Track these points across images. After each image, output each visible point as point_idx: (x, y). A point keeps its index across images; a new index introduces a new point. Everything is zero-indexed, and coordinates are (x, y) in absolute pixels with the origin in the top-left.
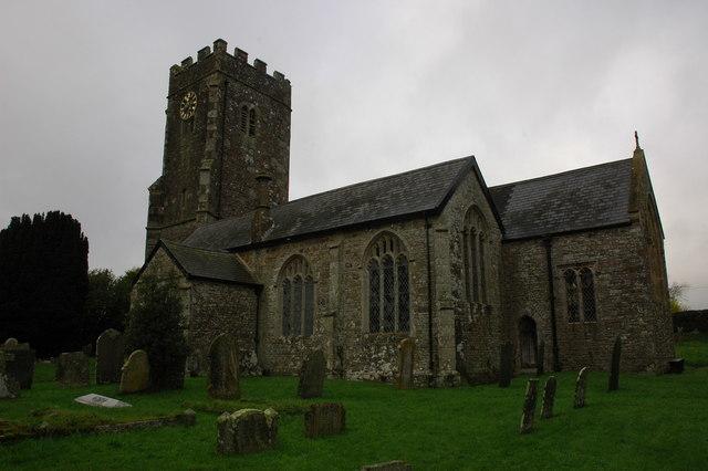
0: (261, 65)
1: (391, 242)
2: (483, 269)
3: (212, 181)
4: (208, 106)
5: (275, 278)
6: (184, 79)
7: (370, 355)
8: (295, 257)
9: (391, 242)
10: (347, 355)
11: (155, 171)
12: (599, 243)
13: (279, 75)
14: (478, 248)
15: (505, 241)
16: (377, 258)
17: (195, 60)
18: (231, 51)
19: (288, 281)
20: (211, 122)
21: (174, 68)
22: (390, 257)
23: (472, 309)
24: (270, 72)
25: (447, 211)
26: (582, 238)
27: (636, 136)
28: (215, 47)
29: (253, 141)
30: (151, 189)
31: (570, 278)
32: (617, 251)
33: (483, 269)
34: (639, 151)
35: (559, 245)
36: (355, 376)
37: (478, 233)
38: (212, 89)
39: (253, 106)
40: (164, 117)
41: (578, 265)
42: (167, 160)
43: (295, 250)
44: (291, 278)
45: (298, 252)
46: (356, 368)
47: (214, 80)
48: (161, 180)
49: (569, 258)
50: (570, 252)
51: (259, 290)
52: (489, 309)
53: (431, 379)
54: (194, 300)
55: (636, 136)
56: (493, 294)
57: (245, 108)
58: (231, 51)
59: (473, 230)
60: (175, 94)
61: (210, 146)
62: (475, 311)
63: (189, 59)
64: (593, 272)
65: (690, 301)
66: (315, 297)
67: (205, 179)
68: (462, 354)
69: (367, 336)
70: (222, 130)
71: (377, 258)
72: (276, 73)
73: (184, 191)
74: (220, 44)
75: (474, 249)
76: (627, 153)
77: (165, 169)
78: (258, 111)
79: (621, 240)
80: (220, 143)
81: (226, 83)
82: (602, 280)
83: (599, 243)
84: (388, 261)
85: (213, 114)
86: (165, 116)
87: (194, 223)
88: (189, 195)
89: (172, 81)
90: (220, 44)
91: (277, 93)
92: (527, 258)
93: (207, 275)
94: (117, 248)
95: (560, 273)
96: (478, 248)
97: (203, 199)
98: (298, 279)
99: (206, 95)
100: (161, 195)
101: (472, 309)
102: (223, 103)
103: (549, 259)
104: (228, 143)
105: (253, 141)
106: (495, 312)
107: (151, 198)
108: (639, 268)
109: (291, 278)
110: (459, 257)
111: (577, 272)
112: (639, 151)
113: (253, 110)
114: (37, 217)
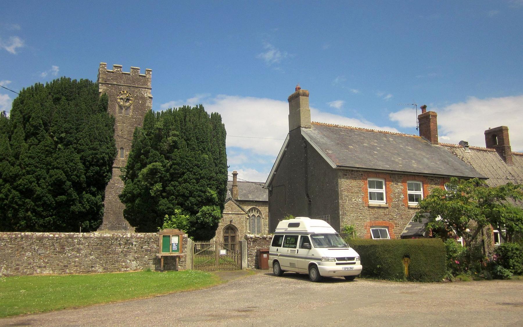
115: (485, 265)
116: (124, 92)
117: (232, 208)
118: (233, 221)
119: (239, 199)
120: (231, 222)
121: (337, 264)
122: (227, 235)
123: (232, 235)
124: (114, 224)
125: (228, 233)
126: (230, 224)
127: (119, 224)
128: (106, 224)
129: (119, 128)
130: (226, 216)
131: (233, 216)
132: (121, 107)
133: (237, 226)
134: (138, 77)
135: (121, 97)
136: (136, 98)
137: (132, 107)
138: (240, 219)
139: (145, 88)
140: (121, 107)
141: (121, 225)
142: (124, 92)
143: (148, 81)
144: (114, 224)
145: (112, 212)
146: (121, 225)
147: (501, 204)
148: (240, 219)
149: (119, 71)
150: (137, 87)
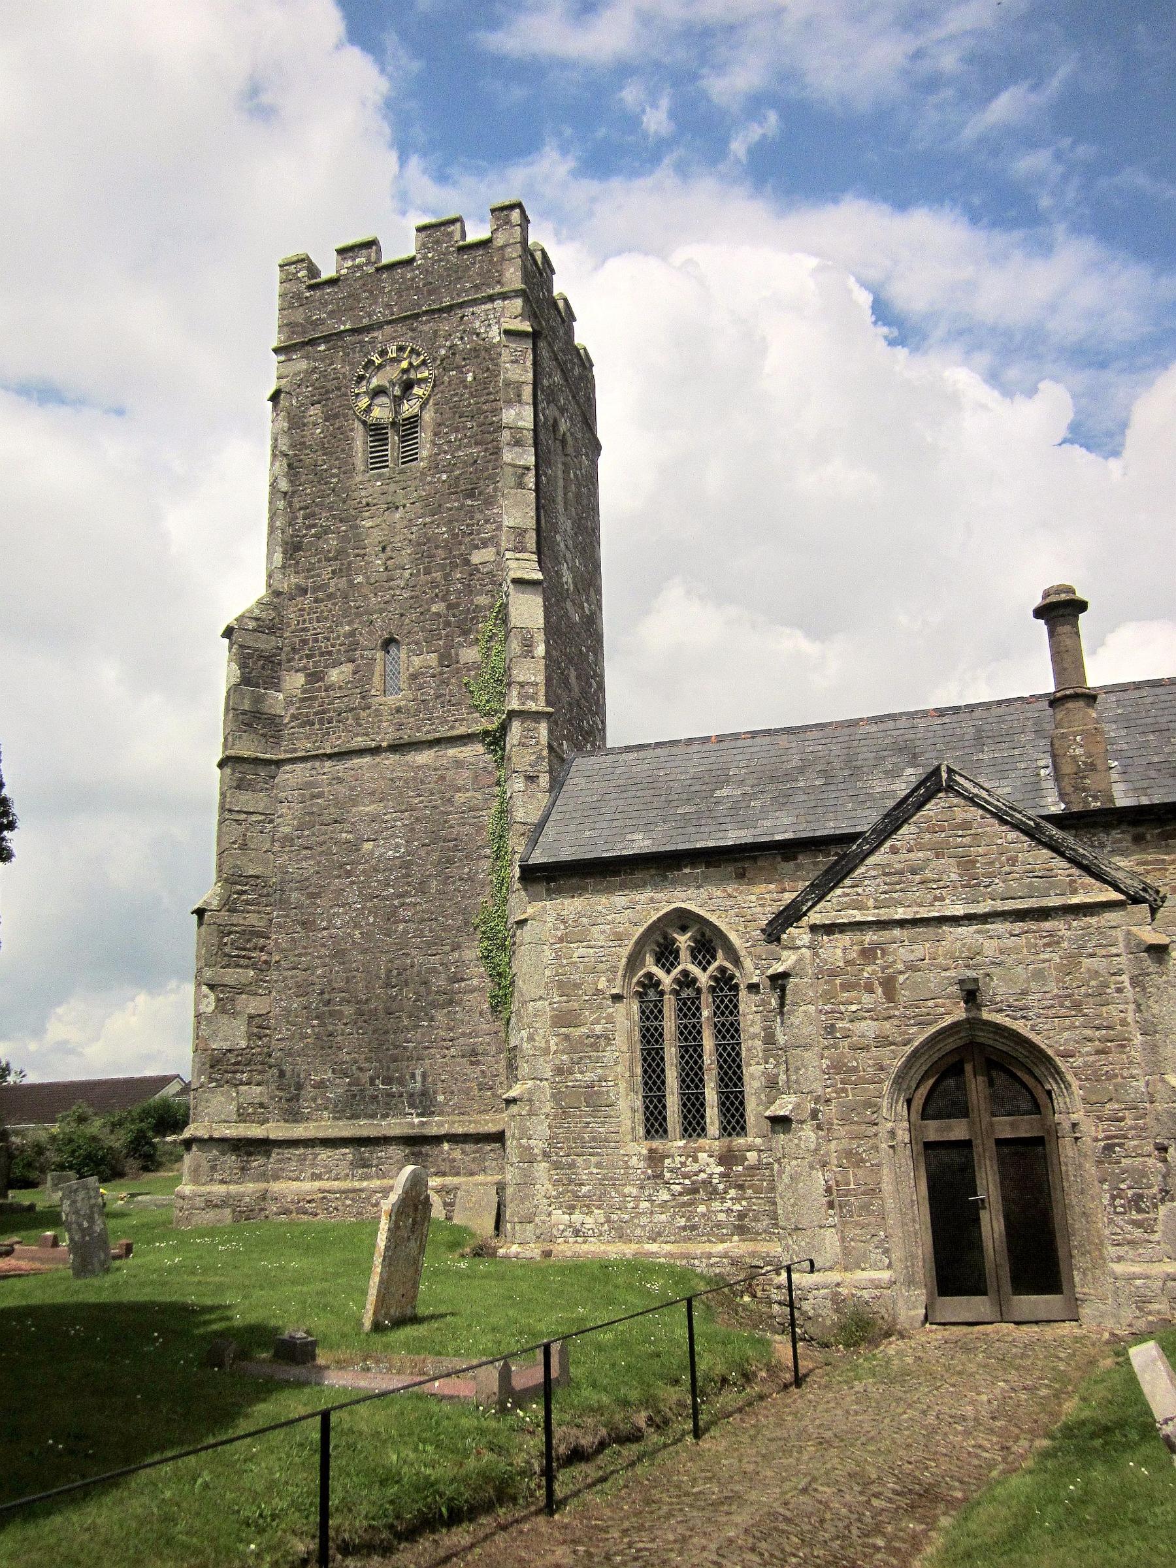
115: (722, 1169)
116: (383, 353)
117: (967, 864)
118: (998, 988)
119: (1123, 800)
120: (971, 995)
121: (403, 463)
122: (958, 1131)
123: (1006, 1127)
124: (364, 1078)
125: (961, 1110)
126: (973, 1023)
127: (388, 1081)
128: (321, 1085)
129: (373, 539)
130: (919, 950)
131: (993, 941)
132: (377, 432)
133: (1046, 1035)
134: (453, 259)
135: (375, 382)
136: (446, 364)
137: (428, 416)
138: (1071, 963)
139: (491, 299)
140: (377, 432)
141: (401, 1082)
142: (383, 353)
143: (503, 259)
144: (364, 1078)
145: (349, 1010)
146: (401, 1082)
147: (820, 1502)
148: (1071, 963)
149: (359, 267)
150: (450, 309)
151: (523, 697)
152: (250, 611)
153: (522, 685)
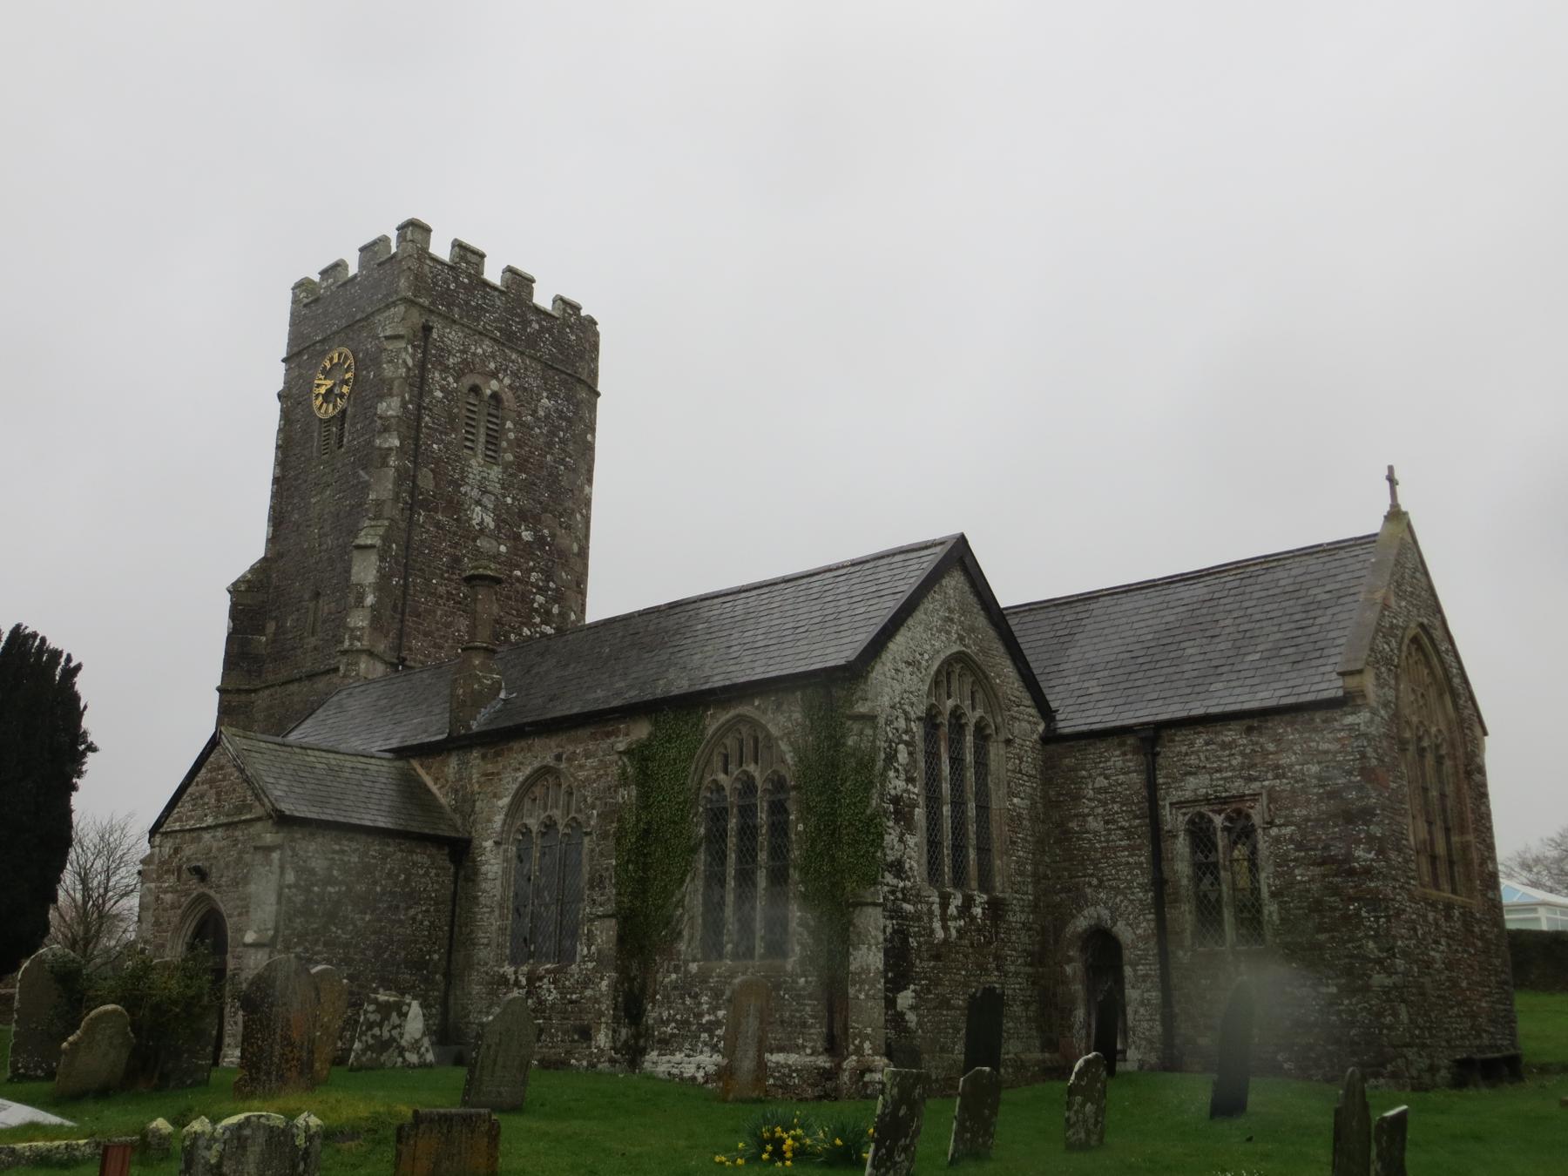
0: (519, 282)
1: (756, 740)
2: (983, 809)
3: (384, 577)
4: (383, 390)
5: (498, 820)
6: (326, 318)
7: (699, 1015)
8: (543, 772)
9: (756, 740)
10: (652, 1015)
11: (249, 543)
12: (1271, 747)
13: (568, 307)
14: (969, 758)
15: (1051, 738)
16: (721, 777)
17: (353, 269)
18: (440, 248)
19: (526, 832)
20: (386, 429)
21: (303, 286)
22: (751, 778)
23: (944, 906)
24: (543, 298)
25: (883, 670)
26: (1229, 735)
27: (1392, 481)
28: (402, 237)
29: (495, 473)
30: (234, 590)
31: (1200, 835)
32: (1315, 769)
33: (983, 809)
34: (1396, 515)
35: (1175, 750)
36: (662, 1069)
37: (972, 717)
38: (390, 346)
39: (494, 385)
40: (276, 407)
41: (1220, 802)
42: (278, 518)
43: (543, 752)
44: (533, 823)
45: (549, 760)
46: (666, 1045)
47: (393, 322)
48: (262, 569)
49: (1195, 785)
50: (1196, 776)
51: (460, 851)
52: (996, 908)
53: (830, 1075)
54: (290, 877)
55: (1392, 481)
56: (1010, 866)
57: (475, 389)
58: (440, 248)
59: (956, 714)
60: (302, 355)
61: (383, 487)
62: (952, 910)
63: (339, 266)
64: (1257, 819)
65: (1531, 904)
66: (586, 869)
67: (365, 571)
68: (911, 1018)
69: (693, 967)
70: (414, 449)
71: (721, 777)
72: (560, 301)
73: (317, 595)
74: (415, 231)
75: (957, 761)
76: (1372, 523)
77: (272, 540)
78: (508, 396)
79: (1325, 743)
80: (406, 478)
81: (427, 329)
82: (1277, 840)
83: (1271, 747)
84: (748, 787)
85: (390, 407)
86: (277, 405)
87: (335, 679)
88: (326, 606)
89: (296, 321)
90: (415, 231)
91: (560, 351)
92: (1101, 782)
93: (329, 815)
94: (1215, 1076)
95: (1174, 820)
96: (969, 758)
97: (359, 620)
98: (549, 826)
99: (375, 361)
100: (254, 603)
101: (944, 906)
102: (419, 382)
103: (1152, 786)
104: (426, 481)
105: (495, 473)
106: (1016, 918)
107: (235, 614)
108: (1366, 814)
109: (533, 823)
110: (910, 780)
111: (1218, 820)
112: (1396, 515)
113: (495, 396)
114: (74, 788)
151: (352, 638)
152: (244, 576)
153: (352, 630)
